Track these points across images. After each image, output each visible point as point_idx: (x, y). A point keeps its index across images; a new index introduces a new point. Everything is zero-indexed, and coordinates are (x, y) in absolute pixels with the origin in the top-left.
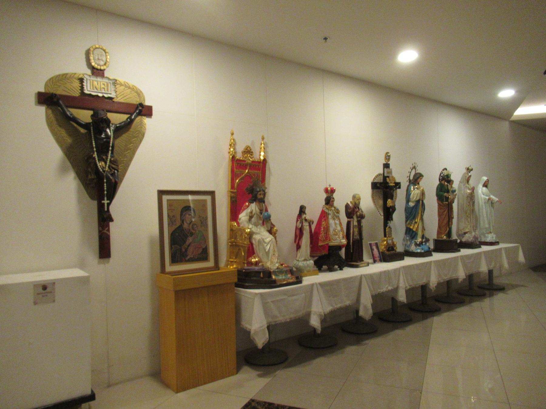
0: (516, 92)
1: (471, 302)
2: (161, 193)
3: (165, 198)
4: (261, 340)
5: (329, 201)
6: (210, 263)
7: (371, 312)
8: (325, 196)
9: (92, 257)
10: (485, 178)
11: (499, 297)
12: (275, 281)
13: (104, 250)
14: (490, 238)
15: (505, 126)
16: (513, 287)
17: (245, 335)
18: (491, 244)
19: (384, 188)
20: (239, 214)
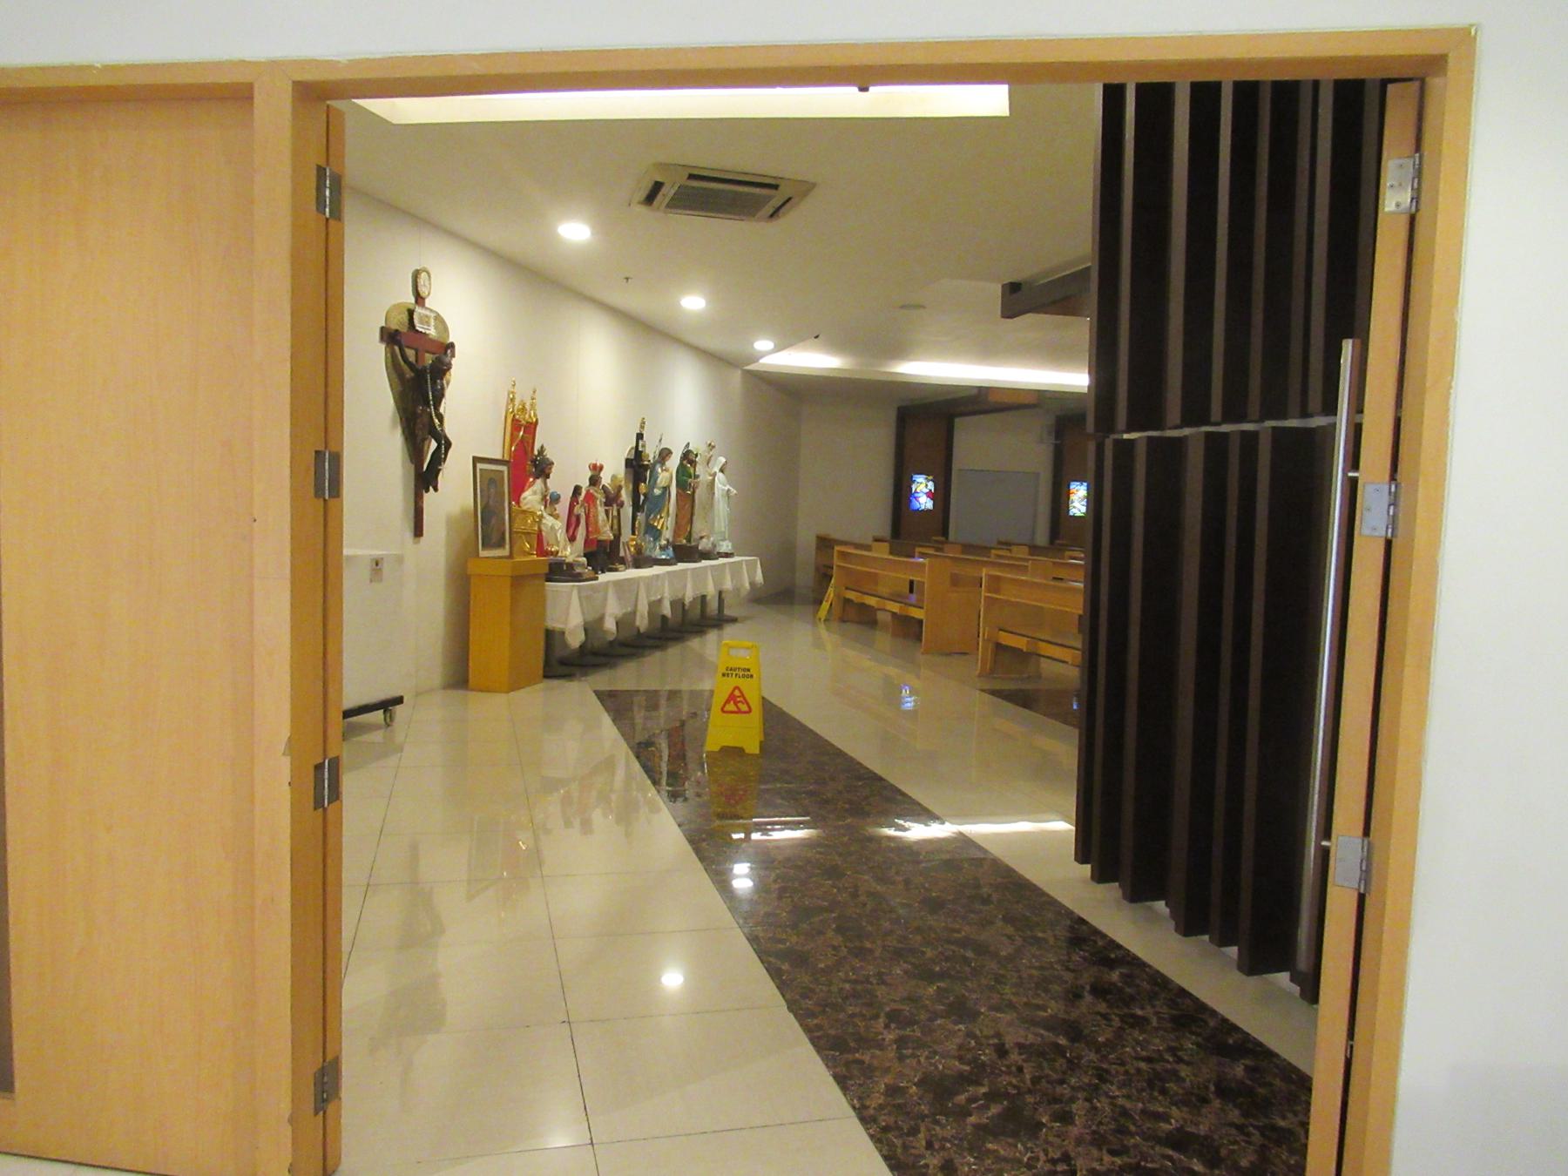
0: (708, 303)
1: (585, 674)
2: (476, 460)
3: (479, 466)
4: (575, 640)
5: (594, 481)
6: (505, 552)
7: (646, 621)
8: (589, 474)
9: (409, 534)
10: (723, 460)
11: (729, 630)
12: (580, 574)
13: (418, 531)
14: (725, 547)
15: (737, 376)
16: (745, 618)
17: (552, 638)
18: (727, 555)
19: (637, 466)
20: (523, 491)
